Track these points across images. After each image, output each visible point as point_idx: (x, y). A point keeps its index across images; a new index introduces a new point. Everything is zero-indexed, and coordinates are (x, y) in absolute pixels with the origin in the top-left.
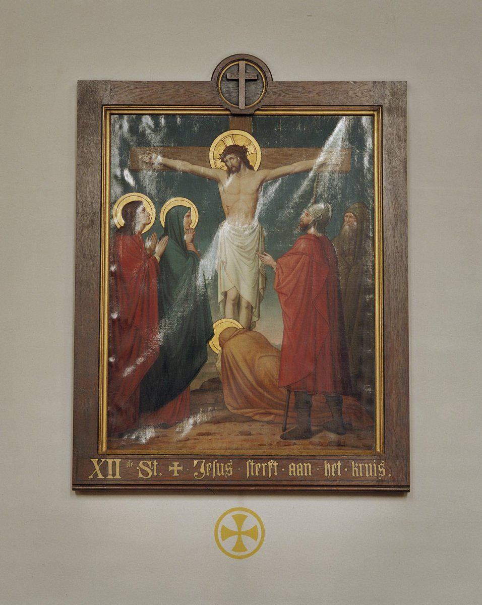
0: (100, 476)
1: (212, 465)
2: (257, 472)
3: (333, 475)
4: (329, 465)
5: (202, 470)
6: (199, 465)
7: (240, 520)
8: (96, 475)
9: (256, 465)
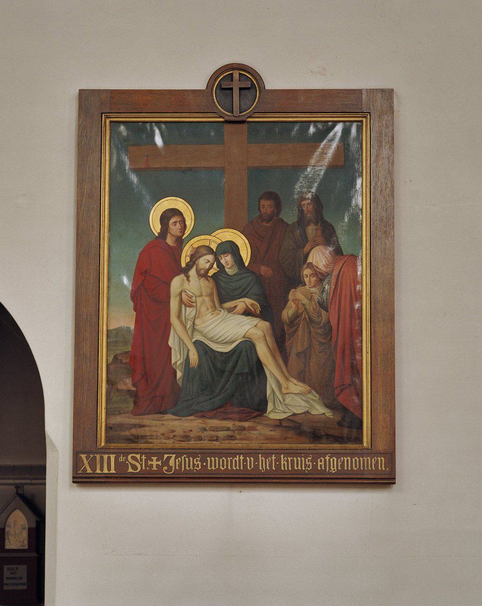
0: (89, 471)
1: (181, 461)
5: (171, 463)
8: (85, 469)
9: (332, 460)
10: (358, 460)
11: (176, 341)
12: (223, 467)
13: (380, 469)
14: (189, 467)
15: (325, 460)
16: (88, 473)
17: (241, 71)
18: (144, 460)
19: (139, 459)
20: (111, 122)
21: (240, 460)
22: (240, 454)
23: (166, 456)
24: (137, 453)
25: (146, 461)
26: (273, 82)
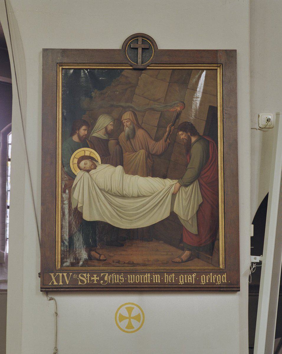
0: (55, 283)
1: (210, 276)
2: (109, 280)
3: (170, 281)
4: (167, 275)
5: (106, 278)
6: (104, 276)
7: (130, 310)
8: (53, 282)
10: (139, 276)
11: (118, 204)
12: (138, 281)
13: (154, 282)
14: (117, 281)
15: (192, 277)
16: (54, 285)
17: (144, 38)
18: (88, 277)
19: (86, 277)
20: (62, 69)
21: (148, 276)
22: (148, 273)
23: (102, 274)
24: (84, 273)
25: (90, 278)
26: (163, 44)
